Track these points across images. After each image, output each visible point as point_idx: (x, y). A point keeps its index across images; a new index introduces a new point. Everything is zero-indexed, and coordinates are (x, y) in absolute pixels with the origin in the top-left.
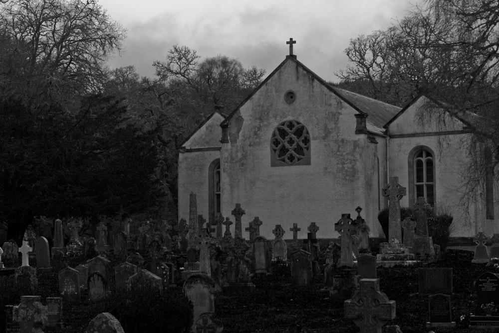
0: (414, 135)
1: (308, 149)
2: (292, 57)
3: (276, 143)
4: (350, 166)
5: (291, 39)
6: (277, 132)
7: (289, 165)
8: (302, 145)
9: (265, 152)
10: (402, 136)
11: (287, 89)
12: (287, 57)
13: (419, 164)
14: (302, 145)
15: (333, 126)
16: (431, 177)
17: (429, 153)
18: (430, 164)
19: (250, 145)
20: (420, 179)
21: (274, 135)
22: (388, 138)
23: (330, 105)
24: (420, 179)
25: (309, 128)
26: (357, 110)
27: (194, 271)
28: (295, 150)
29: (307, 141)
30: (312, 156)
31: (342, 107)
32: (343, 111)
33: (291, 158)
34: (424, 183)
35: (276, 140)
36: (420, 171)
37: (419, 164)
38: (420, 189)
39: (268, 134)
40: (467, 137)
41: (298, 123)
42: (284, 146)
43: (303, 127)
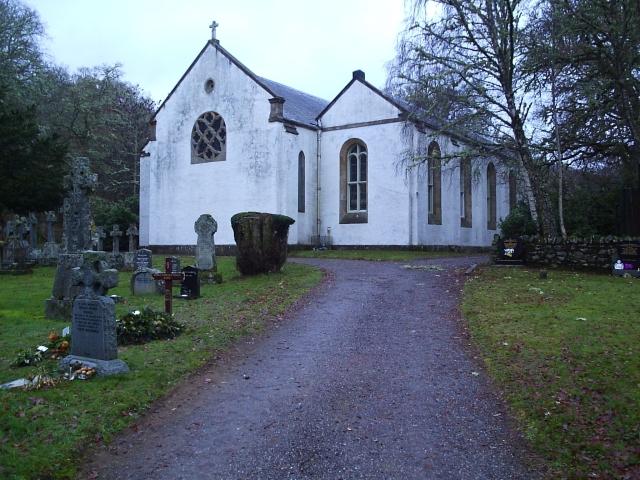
0: (346, 127)
1: (224, 142)
2: (214, 42)
3: (195, 137)
4: (262, 160)
5: (214, 22)
6: (197, 126)
7: (207, 161)
8: (219, 138)
9: (186, 147)
10: (334, 128)
11: (207, 78)
12: (209, 42)
13: (353, 159)
14: (219, 138)
15: (248, 114)
16: (364, 176)
17: (363, 148)
18: (364, 159)
19: (174, 142)
20: (354, 178)
21: (195, 129)
22: (320, 131)
23: (246, 91)
24: (354, 178)
25: (226, 119)
26: (271, 93)
27: (560, 184)
28: (213, 145)
29: (223, 134)
30: (228, 151)
31: (257, 92)
32: (257, 97)
33: (209, 154)
34: (358, 181)
35: (197, 134)
36: (354, 169)
37: (353, 159)
38: (353, 188)
39: (188, 130)
40: (398, 126)
41: (217, 114)
42: (203, 141)
43: (221, 118)
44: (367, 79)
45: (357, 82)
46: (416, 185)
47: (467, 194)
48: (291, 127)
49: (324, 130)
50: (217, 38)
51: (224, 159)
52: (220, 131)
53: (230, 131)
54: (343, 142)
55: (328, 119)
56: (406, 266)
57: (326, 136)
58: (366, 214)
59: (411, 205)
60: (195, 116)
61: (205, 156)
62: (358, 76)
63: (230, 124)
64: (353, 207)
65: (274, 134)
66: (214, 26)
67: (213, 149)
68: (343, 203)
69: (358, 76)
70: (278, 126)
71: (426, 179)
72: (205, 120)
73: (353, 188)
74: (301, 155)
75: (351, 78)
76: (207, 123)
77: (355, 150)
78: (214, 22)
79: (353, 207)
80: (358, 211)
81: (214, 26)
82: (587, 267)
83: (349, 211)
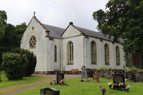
6: (30, 39)
7: (32, 49)
13: (70, 46)
16: (73, 52)
20: (71, 52)
21: (30, 40)
22: (62, 39)
24: (71, 52)
25: (36, 37)
29: (36, 41)
37: (70, 46)
44: (74, 24)
45: (70, 26)
46: (85, 54)
47: (108, 56)
48: (51, 39)
49: (63, 39)
50: (35, 16)
51: (36, 48)
52: (35, 40)
53: (37, 40)
54: (68, 41)
55: (64, 36)
56: (45, 81)
57: (64, 40)
58: (73, 62)
59: (84, 59)
60: (30, 37)
61: (32, 47)
62: (71, 23)
63: (37, 38)
64: (71, 60)
65: (47, 41)
66: (35, 13)
67: (34, 46)
68: (68, 59)
69: (71, 23)
70: (48, 38)
71: (90, 51)
72: (32, 38)
73: (71, 54)
74: (56, 46)
75: (69, 24)
76: (32, 38)
77: (71, 44)
78: (35, 12)
79: (71, 60)
80: (72, 61)
81: (35, 13)
82: (108, 78)
83: (70, 61)
